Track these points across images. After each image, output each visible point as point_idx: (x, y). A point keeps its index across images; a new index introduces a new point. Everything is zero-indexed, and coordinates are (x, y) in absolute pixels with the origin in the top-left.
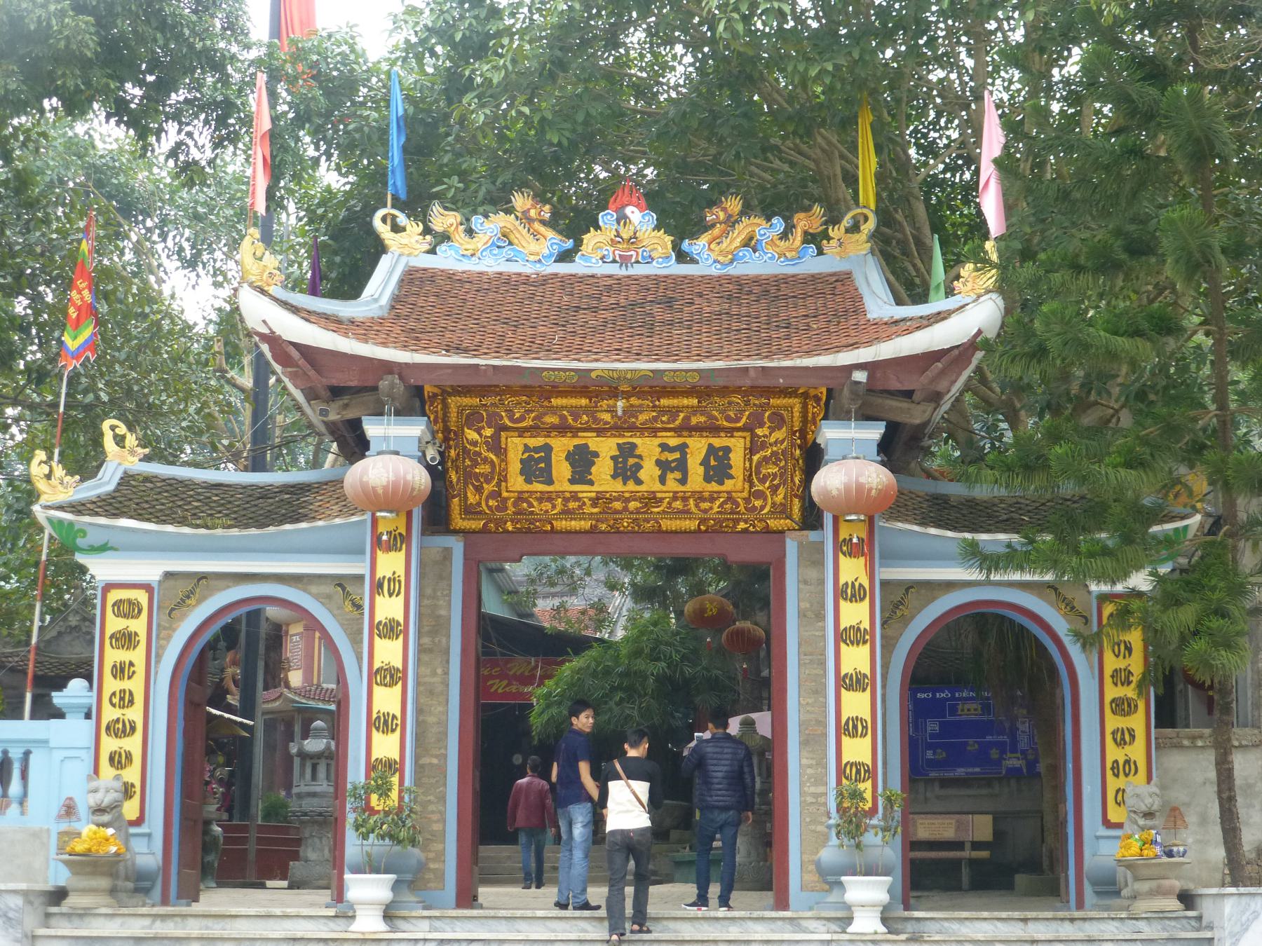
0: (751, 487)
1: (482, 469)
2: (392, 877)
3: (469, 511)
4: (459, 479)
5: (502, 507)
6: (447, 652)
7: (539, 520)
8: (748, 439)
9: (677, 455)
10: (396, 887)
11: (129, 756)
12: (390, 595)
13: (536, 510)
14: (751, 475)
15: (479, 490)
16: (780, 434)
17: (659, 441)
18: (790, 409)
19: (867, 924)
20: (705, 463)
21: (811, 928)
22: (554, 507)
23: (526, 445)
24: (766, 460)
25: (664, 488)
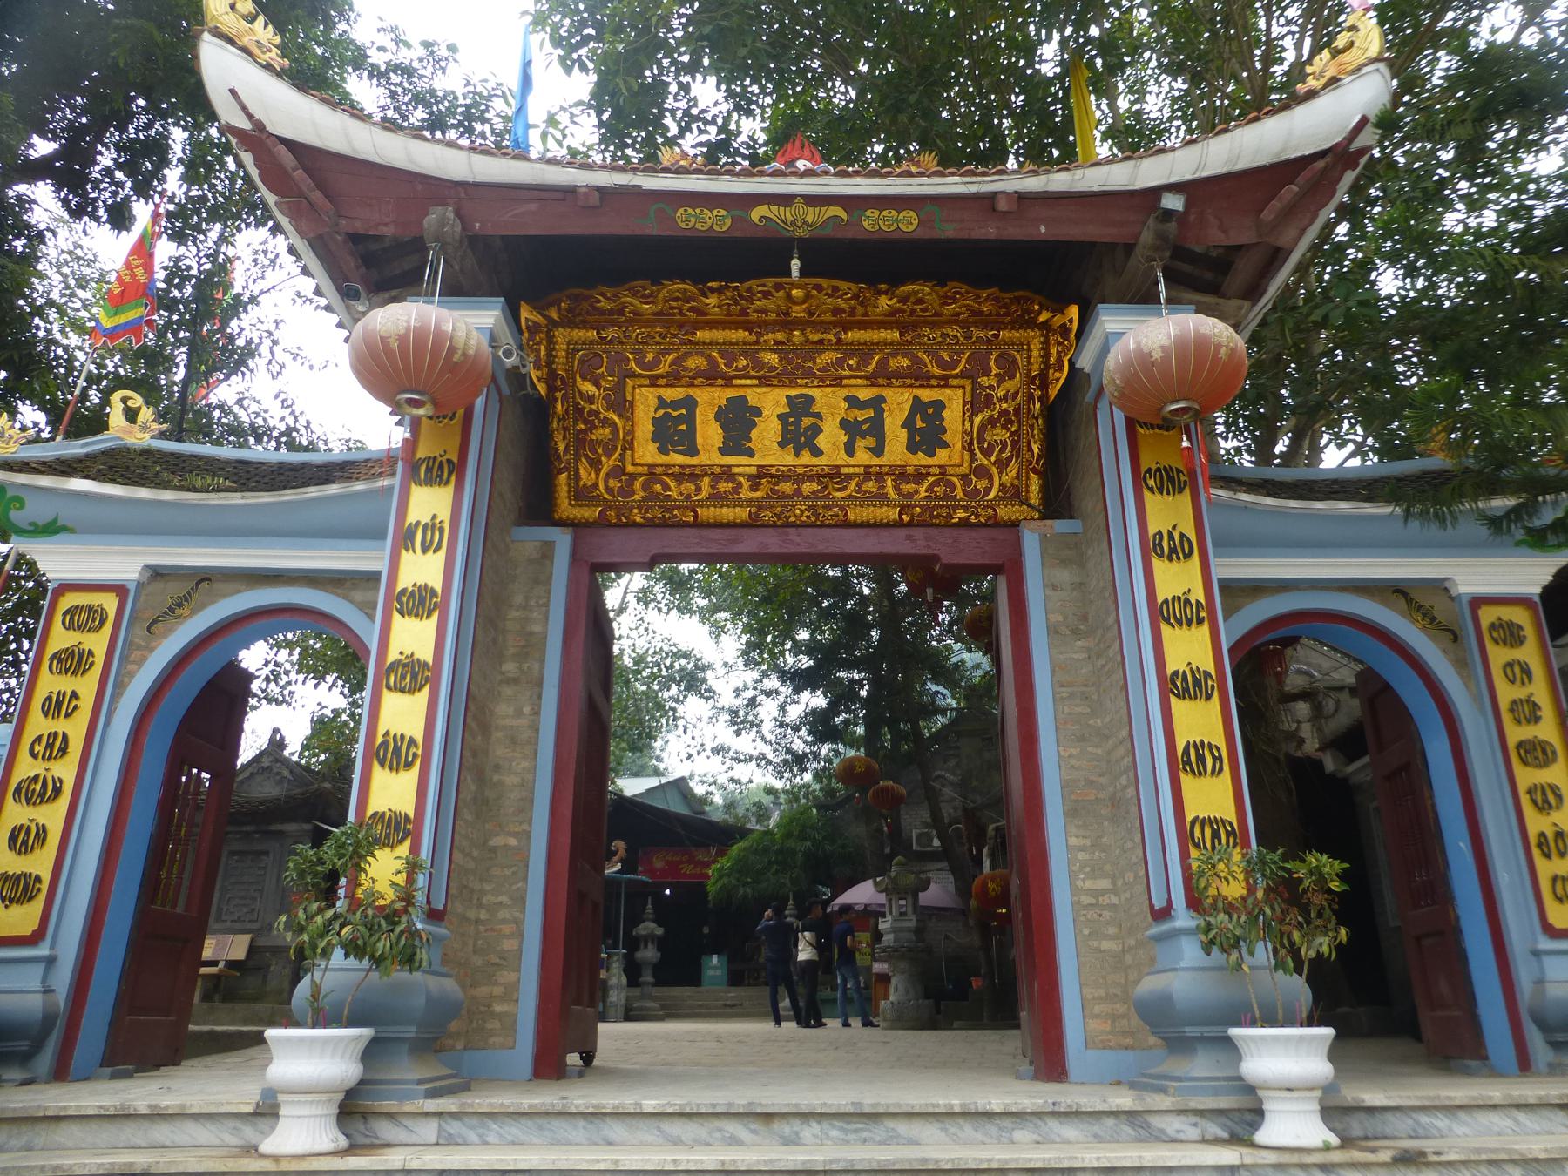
0: (972, 462)
1: (603, 433)
2: (366, 1032)
3: (582, 495)
4: (566, 450)
5: (628, 491)
6: (539, 683)
7: (678, 507)
8: (969, 388)
9: (870, 413)
10: (371, 1054)
11: (42, 833)
12: (425, 550)
13: (674, 494)
14: (971, 443)
15: (596, 465)
16: (1011, 385)
17: (845, 392)
18: (1021, 346)
19: (1293, 1126)
20: (908, 424)
21: (1171, 1132)
22: (698, 490)
23: (660, 398)
24: (992, 422)
25: (852, 461)
